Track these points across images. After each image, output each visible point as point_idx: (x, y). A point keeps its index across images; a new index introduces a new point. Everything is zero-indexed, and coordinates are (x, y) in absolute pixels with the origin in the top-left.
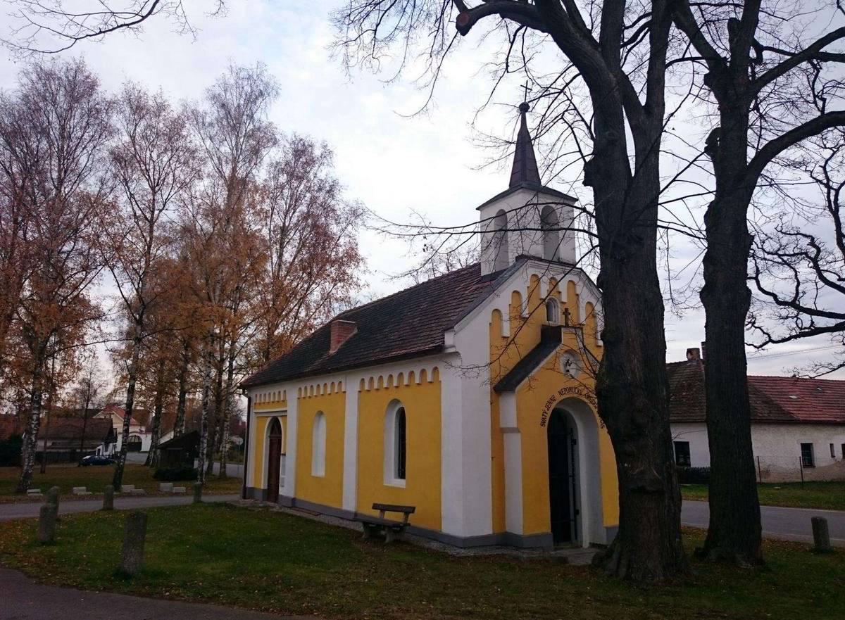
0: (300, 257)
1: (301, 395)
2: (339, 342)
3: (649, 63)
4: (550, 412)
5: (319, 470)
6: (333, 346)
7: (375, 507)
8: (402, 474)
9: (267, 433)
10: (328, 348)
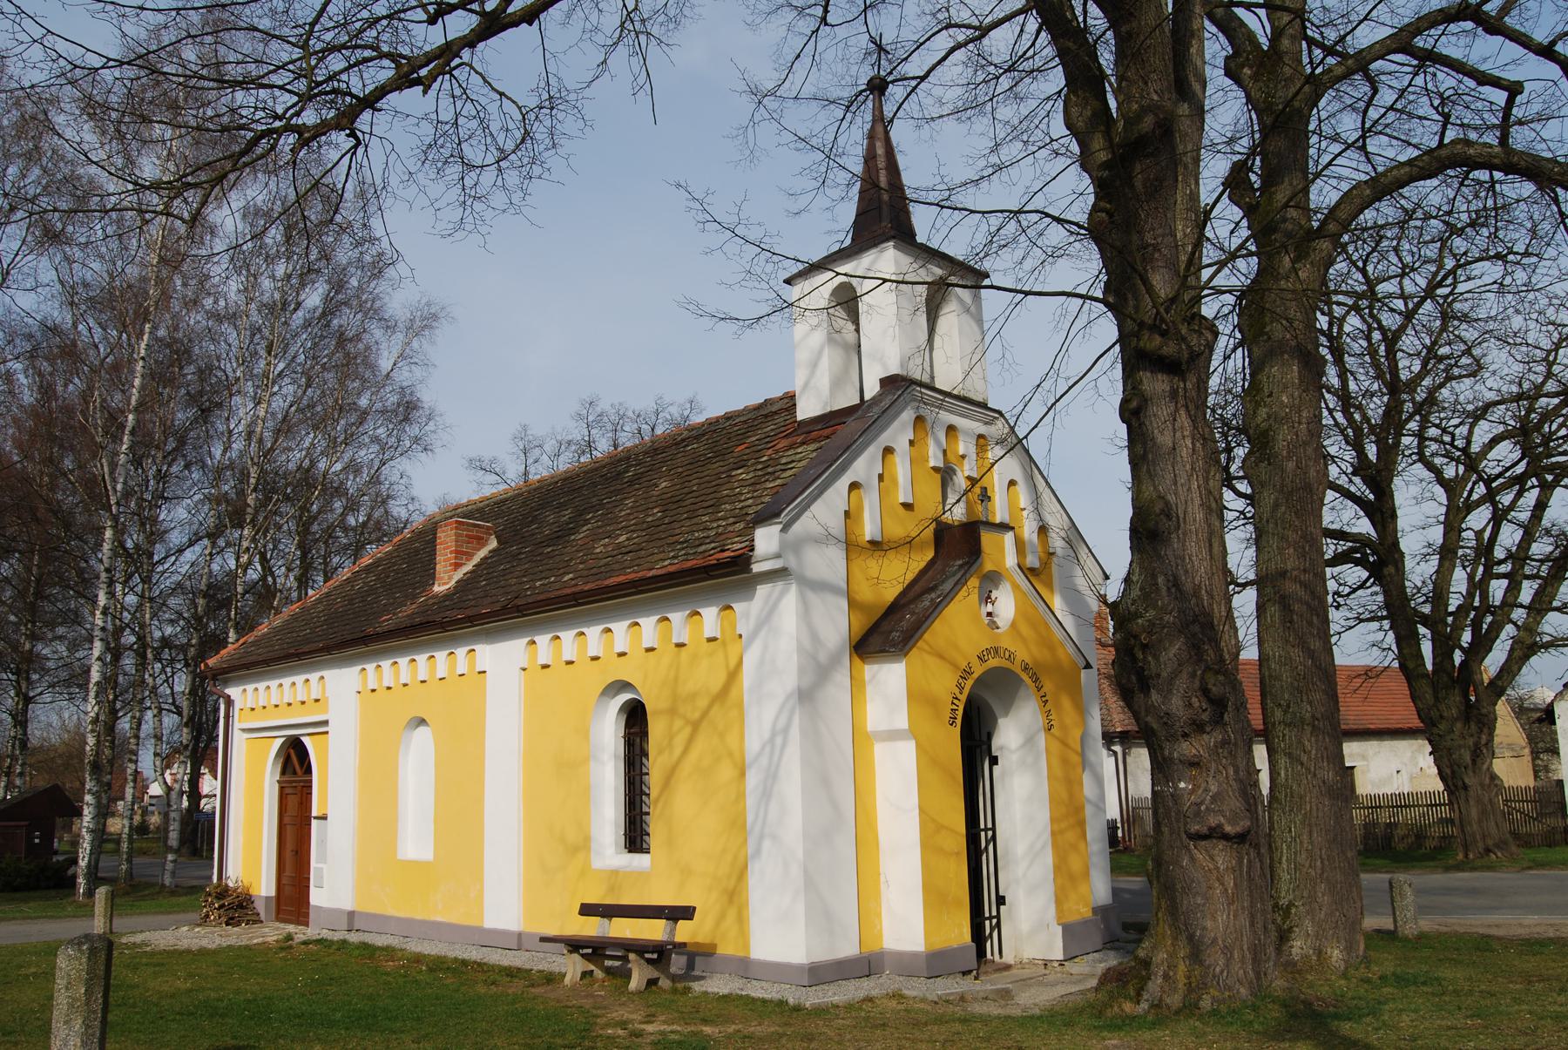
0: (1246, 80)
1: (365, 682)
2: (457, 566)
3: (1055, 40)
4: (964, 697)
5: (416, 843)
6: (442, 566)
7: (587, 910)
8: (635, 839)
9: (272, 773)
10: (430, 576)
